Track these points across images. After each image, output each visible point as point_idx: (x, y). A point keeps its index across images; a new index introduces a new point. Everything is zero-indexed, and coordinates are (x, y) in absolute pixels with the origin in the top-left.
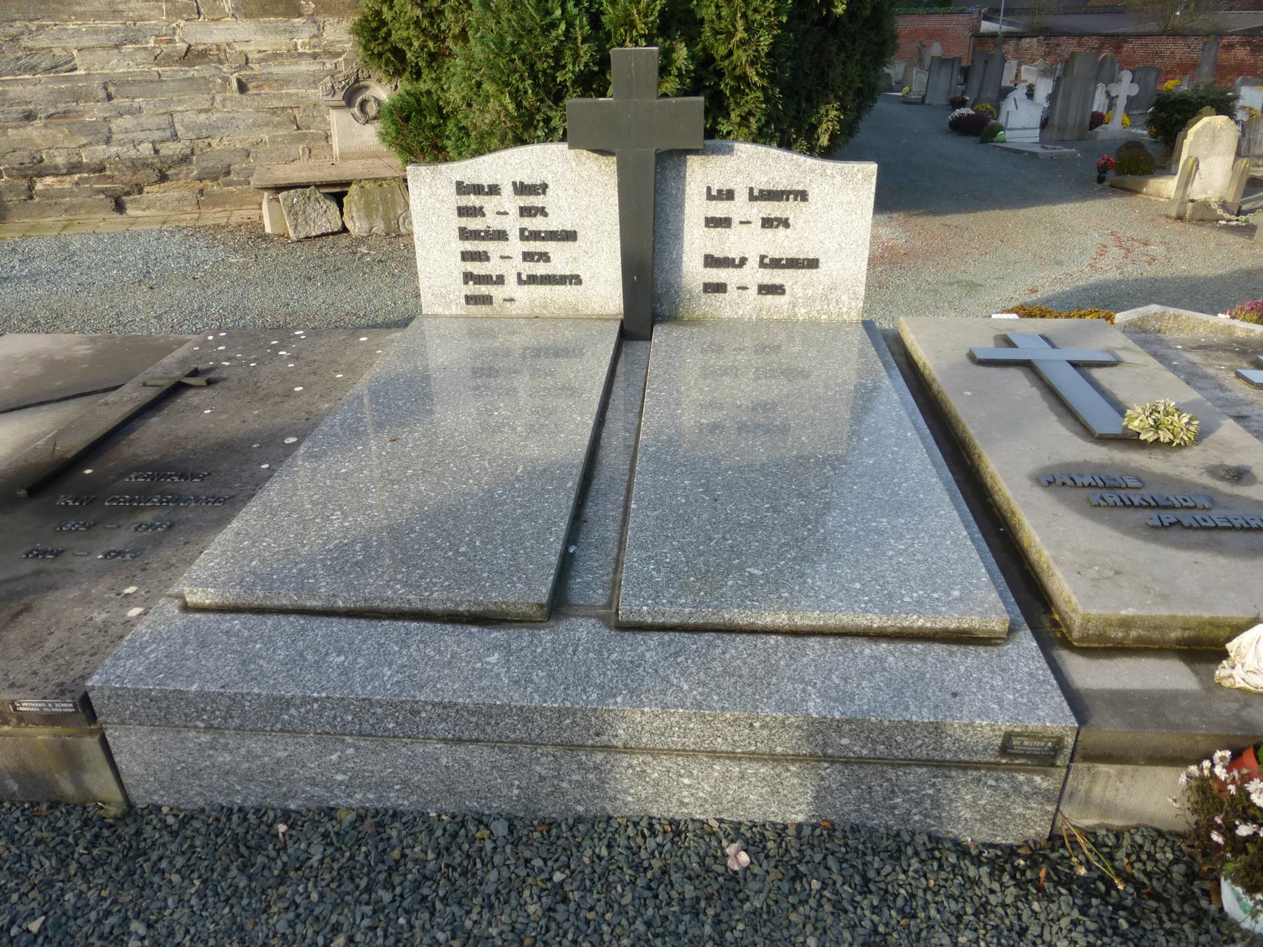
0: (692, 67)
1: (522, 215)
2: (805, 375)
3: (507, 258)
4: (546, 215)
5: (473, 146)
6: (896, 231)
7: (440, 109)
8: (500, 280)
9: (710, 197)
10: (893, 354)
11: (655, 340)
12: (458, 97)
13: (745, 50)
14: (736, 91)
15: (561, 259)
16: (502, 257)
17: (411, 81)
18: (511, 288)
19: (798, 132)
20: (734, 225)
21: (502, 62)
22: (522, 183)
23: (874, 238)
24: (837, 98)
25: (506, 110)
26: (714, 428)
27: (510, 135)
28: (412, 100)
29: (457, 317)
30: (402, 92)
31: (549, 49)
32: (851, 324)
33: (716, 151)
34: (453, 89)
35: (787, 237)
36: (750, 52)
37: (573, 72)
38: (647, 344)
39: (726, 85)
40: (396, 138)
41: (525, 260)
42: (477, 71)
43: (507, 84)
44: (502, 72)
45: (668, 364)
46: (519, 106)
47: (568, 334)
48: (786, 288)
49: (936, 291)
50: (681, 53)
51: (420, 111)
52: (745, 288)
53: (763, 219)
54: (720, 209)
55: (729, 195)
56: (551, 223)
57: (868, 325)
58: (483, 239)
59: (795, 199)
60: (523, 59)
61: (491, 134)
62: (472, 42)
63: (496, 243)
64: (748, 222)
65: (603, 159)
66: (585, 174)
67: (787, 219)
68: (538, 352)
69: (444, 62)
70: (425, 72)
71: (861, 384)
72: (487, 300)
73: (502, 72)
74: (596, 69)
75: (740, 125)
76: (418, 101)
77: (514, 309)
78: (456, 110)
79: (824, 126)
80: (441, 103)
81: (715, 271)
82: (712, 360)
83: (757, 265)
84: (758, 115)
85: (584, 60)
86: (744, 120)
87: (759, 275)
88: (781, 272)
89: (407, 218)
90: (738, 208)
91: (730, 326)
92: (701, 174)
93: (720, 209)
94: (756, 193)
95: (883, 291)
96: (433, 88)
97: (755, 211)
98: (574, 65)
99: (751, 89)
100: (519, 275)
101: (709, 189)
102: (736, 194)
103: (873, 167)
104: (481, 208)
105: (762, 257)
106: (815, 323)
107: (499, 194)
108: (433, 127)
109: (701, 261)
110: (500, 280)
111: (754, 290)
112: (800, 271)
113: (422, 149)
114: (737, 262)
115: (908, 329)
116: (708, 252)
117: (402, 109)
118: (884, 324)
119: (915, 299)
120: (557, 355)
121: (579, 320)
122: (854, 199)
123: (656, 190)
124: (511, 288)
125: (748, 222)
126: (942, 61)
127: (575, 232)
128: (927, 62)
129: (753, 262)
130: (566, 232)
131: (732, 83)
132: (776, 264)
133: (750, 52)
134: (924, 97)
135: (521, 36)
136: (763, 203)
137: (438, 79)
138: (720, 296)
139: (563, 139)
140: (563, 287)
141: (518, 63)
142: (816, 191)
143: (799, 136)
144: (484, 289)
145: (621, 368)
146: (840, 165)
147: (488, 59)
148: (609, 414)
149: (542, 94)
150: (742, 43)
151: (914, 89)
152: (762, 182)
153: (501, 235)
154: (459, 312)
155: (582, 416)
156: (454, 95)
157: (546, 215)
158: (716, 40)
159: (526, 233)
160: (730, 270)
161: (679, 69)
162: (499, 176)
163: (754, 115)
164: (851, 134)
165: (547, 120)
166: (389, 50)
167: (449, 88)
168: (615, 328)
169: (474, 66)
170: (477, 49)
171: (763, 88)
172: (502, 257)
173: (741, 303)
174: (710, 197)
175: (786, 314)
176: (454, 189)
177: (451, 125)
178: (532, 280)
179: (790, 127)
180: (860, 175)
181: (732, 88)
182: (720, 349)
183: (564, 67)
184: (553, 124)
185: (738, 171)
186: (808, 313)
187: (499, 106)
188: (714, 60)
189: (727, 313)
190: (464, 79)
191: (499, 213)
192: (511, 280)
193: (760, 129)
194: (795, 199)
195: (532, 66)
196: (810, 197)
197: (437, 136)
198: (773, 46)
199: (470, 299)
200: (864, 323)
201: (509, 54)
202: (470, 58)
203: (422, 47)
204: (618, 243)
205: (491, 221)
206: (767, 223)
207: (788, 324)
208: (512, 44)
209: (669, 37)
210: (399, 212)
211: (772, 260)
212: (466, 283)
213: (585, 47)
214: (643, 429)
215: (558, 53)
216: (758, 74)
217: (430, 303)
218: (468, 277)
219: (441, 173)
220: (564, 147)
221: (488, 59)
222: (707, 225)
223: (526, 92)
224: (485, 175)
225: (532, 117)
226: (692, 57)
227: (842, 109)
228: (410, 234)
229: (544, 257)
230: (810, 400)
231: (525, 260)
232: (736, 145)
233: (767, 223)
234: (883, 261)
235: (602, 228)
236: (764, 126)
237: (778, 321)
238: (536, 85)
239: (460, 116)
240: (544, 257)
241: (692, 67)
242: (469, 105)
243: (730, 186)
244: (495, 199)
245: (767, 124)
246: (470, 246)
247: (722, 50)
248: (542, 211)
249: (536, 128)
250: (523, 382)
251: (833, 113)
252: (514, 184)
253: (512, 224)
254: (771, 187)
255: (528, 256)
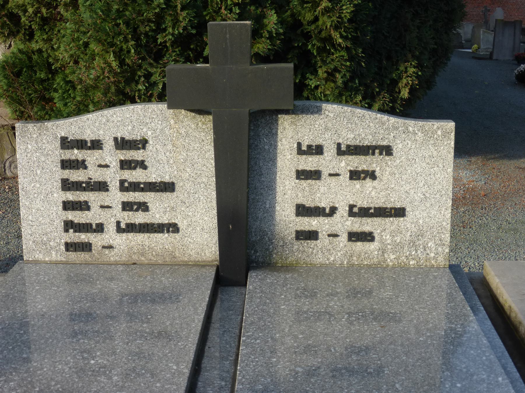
0: (281, 31)
1: (122, 168)
2: (395, 318)
3: (107, 208)
4: (145, 168)
5: (78, 99)
6: (475, 174)
7: (50, 65)
8: (100, 228)
9: (300, 152)
10: (479, 297)
11: (250, 286)
12: (66, 55)
13: (330, 17)
14: (322, 50)
15: (159, 208)
16: (102, 207)
17: (24, 42)
18: (110, 236)
19: (381, 86)
20: (323, 177)
21: (108, 27)
22: (123, 139)
23: (456, 180)
24: (414, 57)
25: (110, 66)
26: (311, 373)
27: (113, 89)
28: (23, 57)
29: (56, 263)
30: (15, 50)
31: (151, 15)
32: (438, 268)
33: (305, 111)
34: (62, 48)
35: (374, 188)
36: (334, 18)
37: (173, 35)
38: (242, 289)
39: (313, 45)
40: (7, 91)
41: (124, 209)
42: (85, 33)
43: (112, 45)
44: (108, 35)
45: (263, 310)
46: (122, 63)
47: (165, 281)
48: (376, 235)
49: (516, 230)
50: (272, 19)
51: (31, 68)
52: (336, 236)
53: (351, 171)
54: (310, 163)
55: (318, 150)
56: (152, 175)
57: (455, 269)
58: (84, 190)
59: (381, 154)
60: (127, 24)
61: (95, 87)
62: (82, 9)
63: (97, 193)
64: (337, 175)
65: (200, 118)
66: (183, 131)
67: (374, 172)
68: (136, 298)
69: (55, 26)
70: (37, 34)
71: (451, 329)
72: (86, 247)
73: (108, 35)
74: (194, 32)
75: (327, 80)
76: (30, 58)
77: (112, 256)
78: (63, 67)
79: (404, 81)
80: (51, 60)
81: (306, 219)
82: (305, 304)
83: (346, 214)
84: (343, 71)
85: (183, 24)
86: (331, 76)
87: (349, 223)
88: (369, 220)
89: (14, 162)
90: (327, 162)
91: (323, 271)
92: (291, 132)
93: (310, 163)
94: (343, 148)
95: (467, 230)
96: (44, 47)
97: (343, 164)
98: (173, 28)
99: (336, 50)
100: (118, 223)
101: (299, 145)
102: (325, 149)
103: (451, 125)
104: (84, 161)
105: (351, 207)
106: (404, 269)
107: (101, 148)
108: (42, 81)
109: (294, 209)
110: (100, 228)
111: (344, 237)
112: (387, 220)
113: (31, 101)
114: (327, 211)
115: (493, 273)
116: (300, 201)
117: (14, 65)
118: (470, 265)
119: (497, 238)
120: (153, 301)
121: (175, 266)
122: (435, 153)
123: (250, 146)
124: (110, 236)
125: (337, 175)
126: (505, 24)
127: (173, 184)
128: (492, 24)
129: (343, 211)
130: (165, 183)
131: (319, 45)
132: (365, 213)
133: (334, 18)
134: (491, 54)
135: (126, 4)
136: (350, 158)
137: (50, 40)
138: (312, 243)
139: (161, 98)
140: (161, 235)
141: (123, 27)
142: (400, 146)
143: (381, 90)
144: (83, 237)
145: (216, 314)
146: (421, 123)
147: (95, 24)
148: (206, 363)
149: (144, 53)
150: (327, 10)
151: (482, 47)
152: (348, 138)
153: (102, 187)
154: (59, 258)
155: (177, 364)
156: (63, 53)
157: (145, 168)
158: (303, 8)
159: (126, 184)
160: (321, 219)
161: (270, 33)
162: (101, 132)
163: (339, 72)
164: (429, 88)
165: (148, 76)
166: (6, 15)
167: (59, 47)
168: (211, 274)
169: (82, 29)
170: (86, 16)
171: (347, 49)
172: (102, 207)
173: (332, 250)
174: (300, 152)
175: (375, 260)
176: (58, 144)
177: (59, 79)
178: (131, 228)
179: (372, 81)
180: (439, 133)
181: (318, 48)
182: (313, 295)
183: (165, 30)
184: (153, 79)
185: (327, 129)
186: (397, 258)
187: (102, 64)
188: (301, 25)
189: (319, 259)
190: (73, 40)
191: (100, 166)
192: (111, 228)
193: (345, 83)
194: (381, 154)
195: (135, 30)
196: (395, 152)
197: (45, 89)
198: (355, 13)
199: (70, 247)
200: (451, 267)
201: (115, 19)
202: (80, 22)
203: (36, 13)
204: (214, 194)
205: (94, 174)
206: (355, 175)
207: (378, 269)
208: (118, 10)
209: (260, 5)
210: (6, 157)
211: (361, 209)
212: (66, 231)
213: (184, 13)
214: (238, 378)
215: (159, 18)
216: (342, 37)
217: (31, 250)
218: (69, 225)
219: (47, 129)
220: (163, 106)
221: (95, 24)
222: (298, 178)
223: (129, 52)
224: (89, 132)
225: (134, 73)
226: (281, 22)
227: (420, 66)
228: (15, 177)
229: (143, 207)
230: (402, 345)
231: (124, 209)
232: (324, 106)
233: (355, 175)
234: (464, 201)
235: (199, 180)
236: (348, 81)
237: (369, 266)
238: (138, 46)
239: (67, 72)
240: (143, 207)
241: (281, 31)
242: (76, 62)
243: (319, 141)
244: (97, 153)
245: (352, 79)
246: (71, 196)
247: (309, 17)
248: (142, 164)
249: (137, 83)
250: (120, 328)
251: (411, 70)
252: (116, 139)
253: (113, 176)
254: (357, 143)
255: (127, 206)
